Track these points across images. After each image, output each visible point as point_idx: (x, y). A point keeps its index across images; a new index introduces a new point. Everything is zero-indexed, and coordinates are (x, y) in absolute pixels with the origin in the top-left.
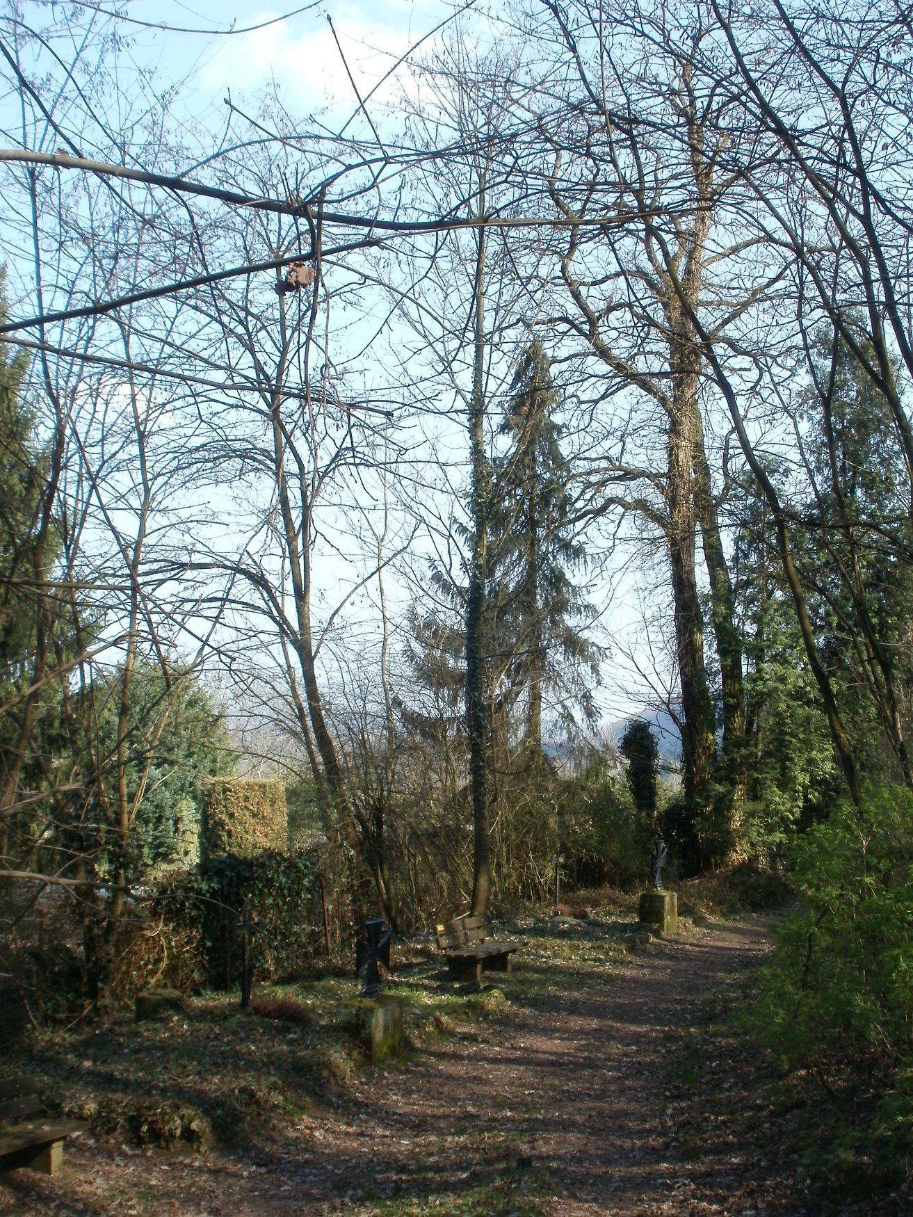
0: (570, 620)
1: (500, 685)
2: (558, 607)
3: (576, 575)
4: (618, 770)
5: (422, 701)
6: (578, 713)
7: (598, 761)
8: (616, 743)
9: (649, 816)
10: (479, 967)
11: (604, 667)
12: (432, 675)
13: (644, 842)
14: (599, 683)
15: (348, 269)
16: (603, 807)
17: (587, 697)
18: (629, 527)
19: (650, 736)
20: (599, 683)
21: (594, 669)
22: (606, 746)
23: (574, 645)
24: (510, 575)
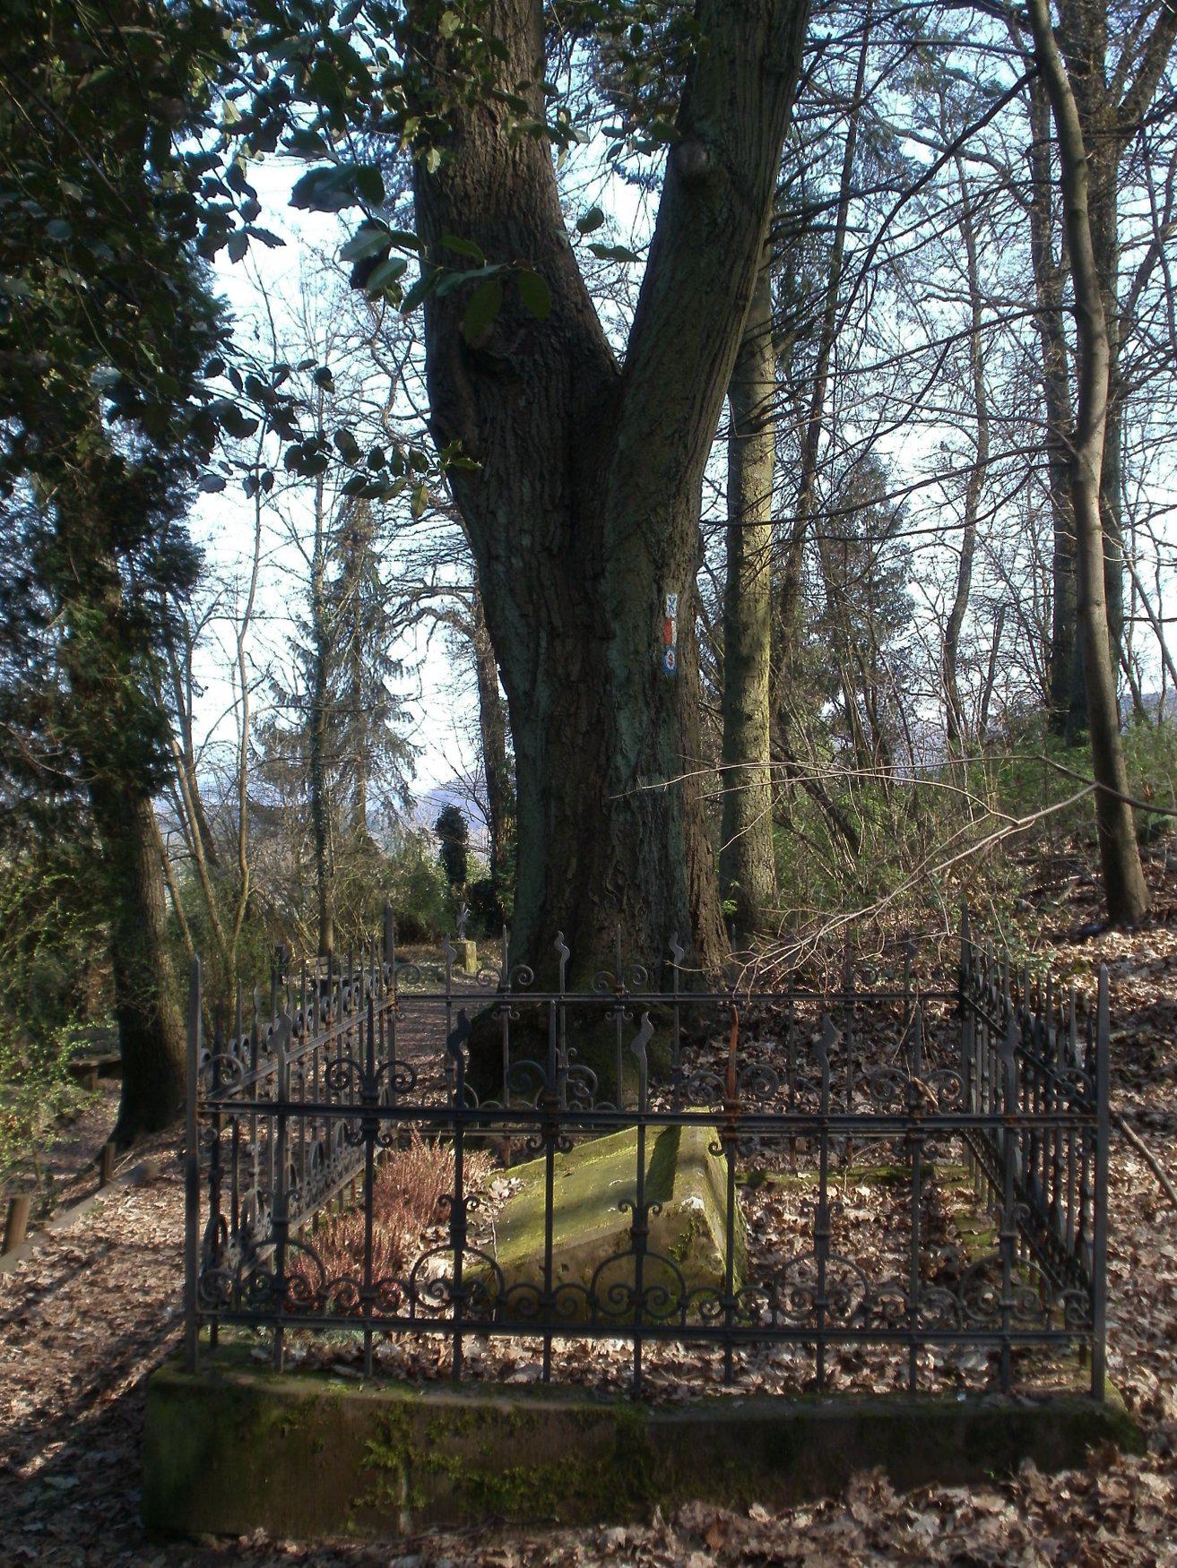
0: (391, 724)
1: (331, 778)
2: (382, 714)
3: (394, 685)
4: (433, 851)
5: (271, 796)
6: (397, 803)
7: (415, 841)
8: (430, 827)
9: (459, 889)
10: (95, 1075)
11: (419, 762)
12: (272, 771)
13: (453, 908)
14: (414, 776)
15: (257, 539)
16: (420, 879)
17: (405, 788)
18: (443, 631)
19: (461, 820)
20: (414, 776)
21: (410, 765)
22: (423, 831)
23: (396, 746)
24: (339, 683)
